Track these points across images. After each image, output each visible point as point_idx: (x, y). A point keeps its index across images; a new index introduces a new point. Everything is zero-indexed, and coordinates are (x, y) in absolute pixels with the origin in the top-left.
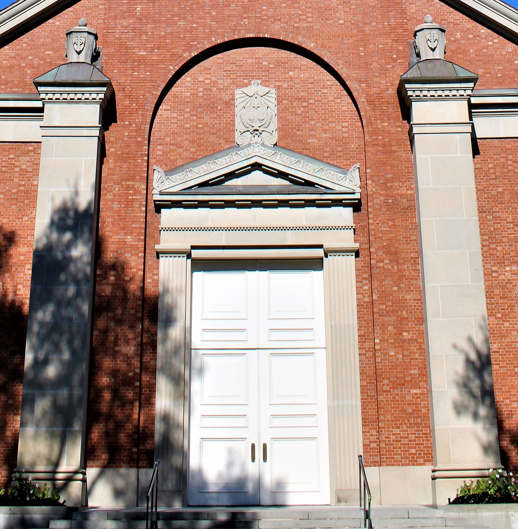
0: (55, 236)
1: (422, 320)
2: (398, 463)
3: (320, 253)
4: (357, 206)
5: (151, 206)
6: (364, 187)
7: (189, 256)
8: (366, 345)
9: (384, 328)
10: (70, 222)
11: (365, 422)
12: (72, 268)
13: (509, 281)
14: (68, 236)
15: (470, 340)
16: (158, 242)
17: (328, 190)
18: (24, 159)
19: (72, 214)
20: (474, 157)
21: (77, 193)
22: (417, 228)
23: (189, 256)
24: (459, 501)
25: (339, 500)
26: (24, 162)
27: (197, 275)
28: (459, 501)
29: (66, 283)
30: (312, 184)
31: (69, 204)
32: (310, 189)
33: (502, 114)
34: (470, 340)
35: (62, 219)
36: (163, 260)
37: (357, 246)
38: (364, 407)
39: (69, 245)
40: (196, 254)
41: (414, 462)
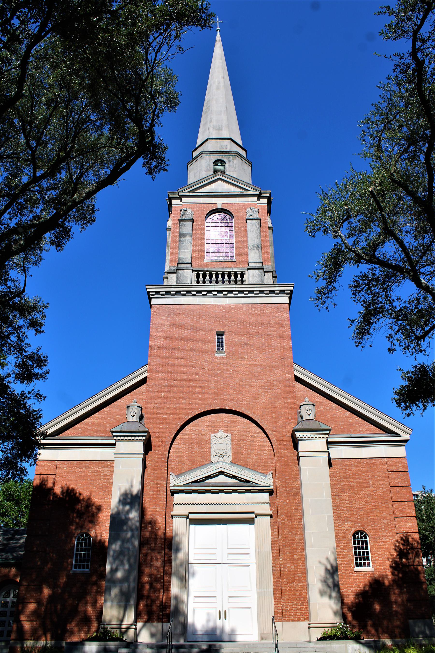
0: (121, 507)
2: (292, 620)
3: (253, 516)
4: (271, 493)
6: (275, 483)
8: (276, 562)
9: (285, 552)
10: (129, 500)
12: (130, 523)
13: (347, 530)
14: (127, 507)
17: (257, 485)
19: (129, 496)
21: (132, 486)
25: (262, 639)
27: (192, 527)
29: (126, 531)
31: (128, 492)
32: (248, 484)
38: (275, 592)
39: (128, 512)
41: (299, 620)
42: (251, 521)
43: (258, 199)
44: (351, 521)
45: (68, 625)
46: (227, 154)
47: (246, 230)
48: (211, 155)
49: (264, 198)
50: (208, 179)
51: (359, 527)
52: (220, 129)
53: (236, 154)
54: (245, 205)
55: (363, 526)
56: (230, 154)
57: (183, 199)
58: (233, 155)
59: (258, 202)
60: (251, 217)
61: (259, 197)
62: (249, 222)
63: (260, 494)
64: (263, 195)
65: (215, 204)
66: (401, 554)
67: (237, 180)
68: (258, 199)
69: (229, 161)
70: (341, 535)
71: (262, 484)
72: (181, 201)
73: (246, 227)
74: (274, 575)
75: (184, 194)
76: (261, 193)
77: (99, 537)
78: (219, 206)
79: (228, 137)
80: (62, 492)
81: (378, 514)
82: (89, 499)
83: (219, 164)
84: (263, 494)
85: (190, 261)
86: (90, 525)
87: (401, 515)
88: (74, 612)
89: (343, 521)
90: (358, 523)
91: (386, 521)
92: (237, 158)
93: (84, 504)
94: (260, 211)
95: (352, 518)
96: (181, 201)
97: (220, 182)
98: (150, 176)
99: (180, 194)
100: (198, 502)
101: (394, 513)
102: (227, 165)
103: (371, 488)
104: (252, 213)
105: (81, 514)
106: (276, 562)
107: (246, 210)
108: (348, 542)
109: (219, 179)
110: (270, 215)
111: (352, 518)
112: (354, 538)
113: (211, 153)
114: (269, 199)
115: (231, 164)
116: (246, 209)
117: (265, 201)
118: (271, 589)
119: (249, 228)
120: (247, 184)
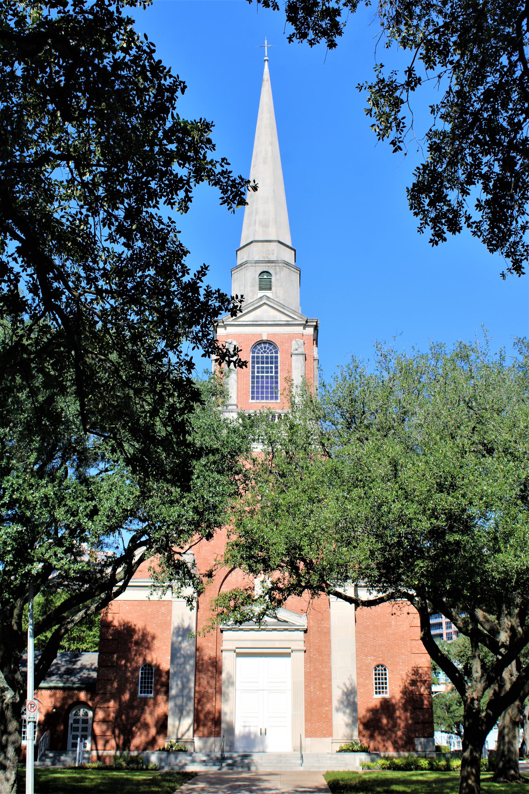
0: (175, 638)
1: (330, 680)
2: (318, 737)
3: (289, 651)
4: (306, 631)
5: (219, 630)
6: (308, 623)
7: (235, 651)
8: (308, 690)
9: (315, 682)
10: (181, 633)
11: (306, 720)
12: (182, 652)
13: (370, 663)
14: (180, 639)
15: (345, 684)
16: (222, 646)
17: (294, 624)
18: (163, 608)
19: (181, 630)
20: (356, 610)
21: (183, 620)
22: (330, 641)
23: (235, 651)
24: (340, 751)
25: (295, 750)
26: (163, 610)
27: (238, 659)
28: (340, 751)
29: (179, 658)
30: (287, 622)
31: (180, 625)
32: (286, 624)
33: (139, 590)
34: (345, 684)
35: (178, 632)
36: (224, 653)
37: (305, 648)
38: (306, 714)
39: (180, 643)
40: (238, 651)
41: (325, 736)
42: (288, 655)
43: (304, 328)
44: (374, 656)
45: (123, 697)
46: (274, 264)
47: (291, 366)
48: (257, 265)
49: (310, 326)
50: (253, 305)
51: (380, 661)
52: (266, 226)
53: (283, 265)
54: (291, 337)
55: (383, 660)
56: (277, 264)
57: (227, 328)
58: (280, 265)
59: (304, 331)
60: (296, 352)
61: (305, 326)
62: (293, 357)
63: (296, 632)
64: (309, 324)
65: (260, 335)
66: (413, 683)
67: (283, 306)
68: (304, 328)
69: (276, 274)
70: (364, 668)
71: (297, 624)
72: (226, 329)
73: (291, 362)
74: (305, 701)
75: (229, 323)
76: (307, 322)
77: (154, 662)
78: (265, 338)
79: (276, 239)
80: (120, 624)
81: (397, 651)
82: (144, 629)
83: (265, 277)
84: (299, 632)
85: (235, 403)
86: (147, 651)
87: (417, 652)
88: (137, 719)
89: (367, 656)
90: (379, 658)
91: (403, 657)
92: (285, 268)
93: (141, 634)
94: (306, 342)
95: (375, 654)
96: (226, 329)
97: (265, 307)
98: (193, 361)
99: (225, 323)
100: (243, 638)
101: (411, 650)
102: (273, 279)
103: (393, 627)
104: (297, 347)
105: (137, 643)
106: (308, 690)
107: (291, 342)
108: (370, 674)
109: (265, 304)
110: (317, 344)
111: (375, 654)
112: (376, 670)
113: (257, 262)
114: (316, 328)
115: (278, 276)
116: (291, 341)
117: (310, 331)
118: (303, 712)
119: (293, 364)
120: (294, 312)
